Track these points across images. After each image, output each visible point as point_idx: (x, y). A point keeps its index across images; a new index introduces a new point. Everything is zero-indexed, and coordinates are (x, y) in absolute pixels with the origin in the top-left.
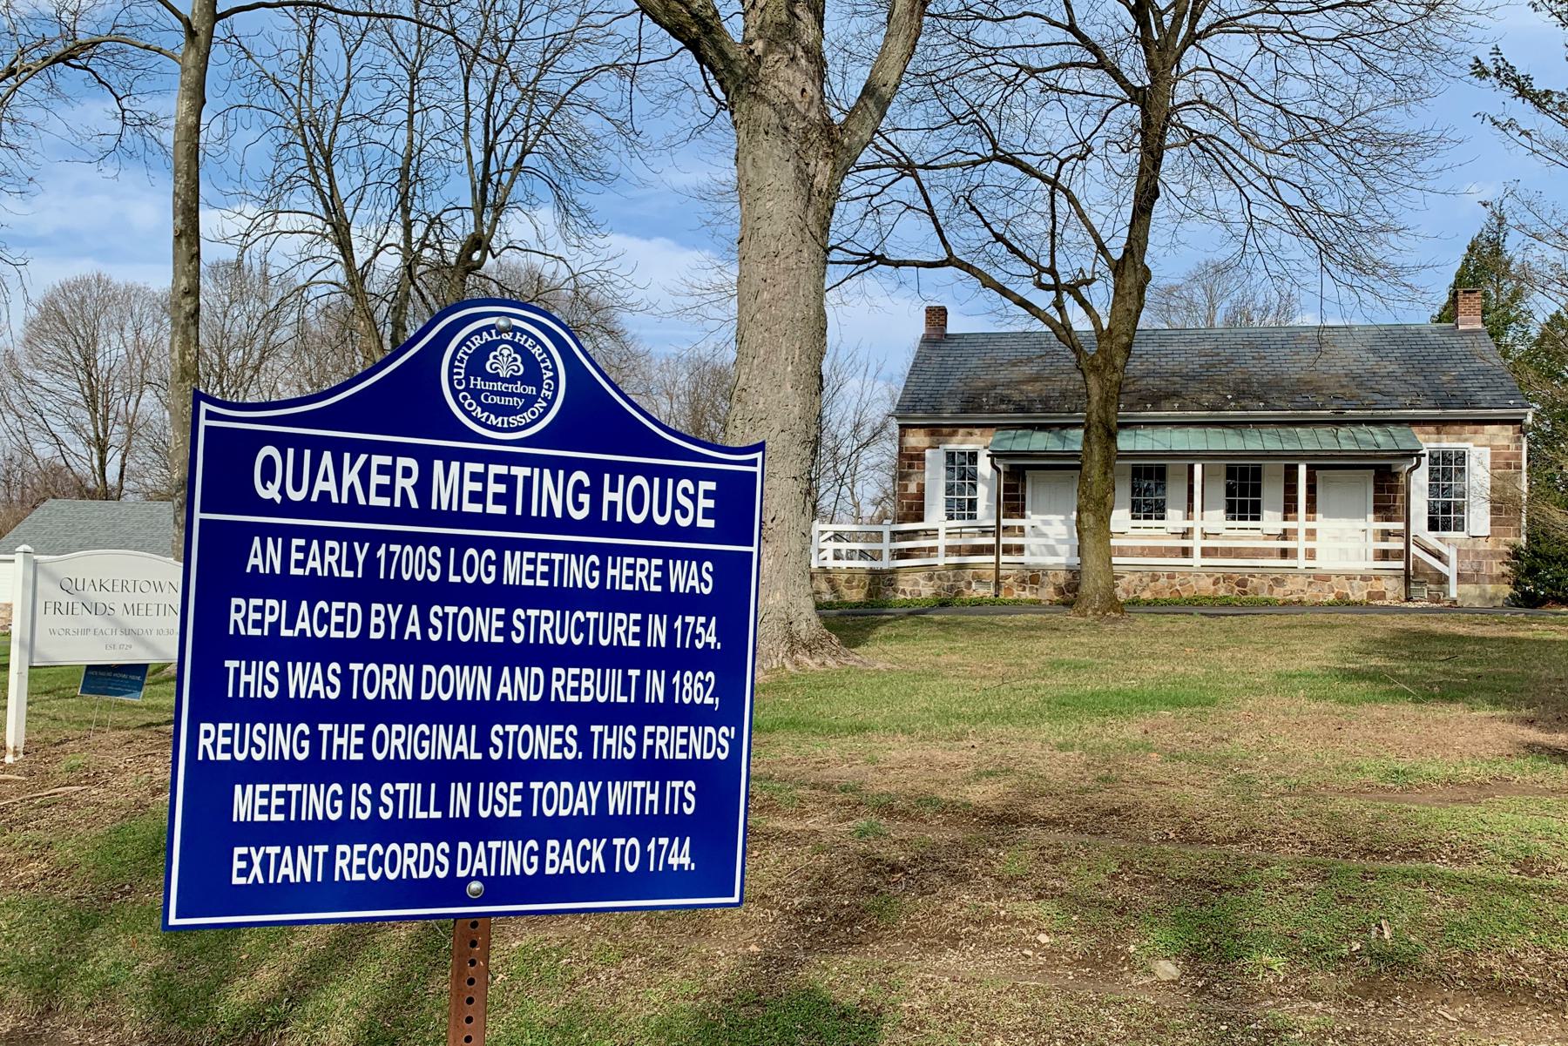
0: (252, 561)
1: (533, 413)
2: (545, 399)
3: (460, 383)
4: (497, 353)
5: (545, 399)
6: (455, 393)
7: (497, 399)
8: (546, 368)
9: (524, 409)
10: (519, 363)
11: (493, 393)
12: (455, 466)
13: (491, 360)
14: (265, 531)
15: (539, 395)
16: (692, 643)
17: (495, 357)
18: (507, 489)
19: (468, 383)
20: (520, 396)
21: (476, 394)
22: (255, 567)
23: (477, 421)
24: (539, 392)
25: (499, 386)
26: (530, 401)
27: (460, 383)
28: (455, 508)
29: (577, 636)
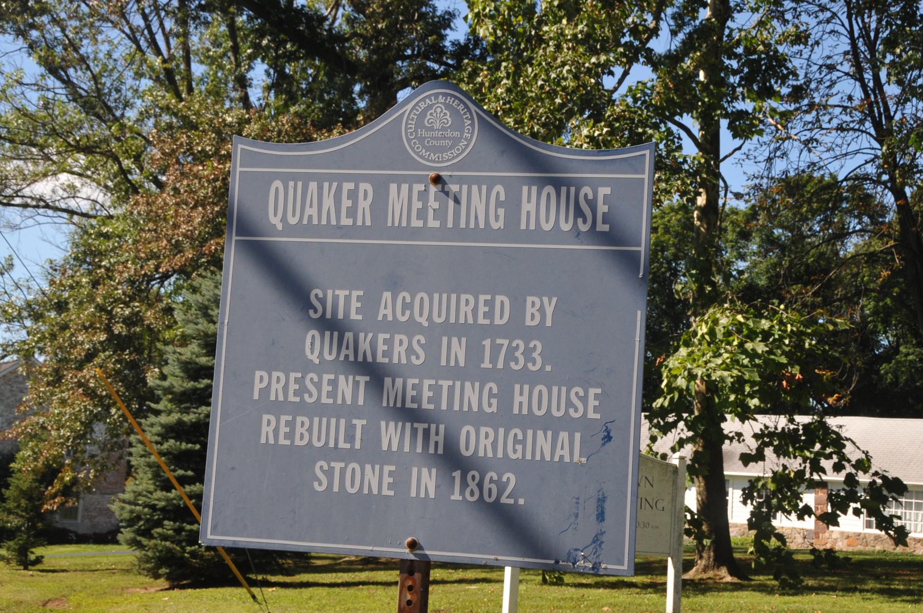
0: (382, 312)
1: (458, 149)
2: (466, 139)
3: (411, 134)
4: (432, 111)
5: (466, 139)
6: (409, 140)
7: (435, 142)
8: (467, 118)
9: (451, 148)
10: (447, 117)
11: (432, 138)
12: (405, 187)
13: (429, 117)
14: (277, 176)
15: (461, 138)
16: (506, 363)
17: (431, 114)
18: (393, 182)
19: (417, 134)
20: (450, 139)
21: (422, 140)
22: (385, 316)
23: (422, 157)
24: (462, 135)
25: (435, 134)
26: (456, 141)
27: (411, 134)
28: (404, 224)
29: (403, 314)
